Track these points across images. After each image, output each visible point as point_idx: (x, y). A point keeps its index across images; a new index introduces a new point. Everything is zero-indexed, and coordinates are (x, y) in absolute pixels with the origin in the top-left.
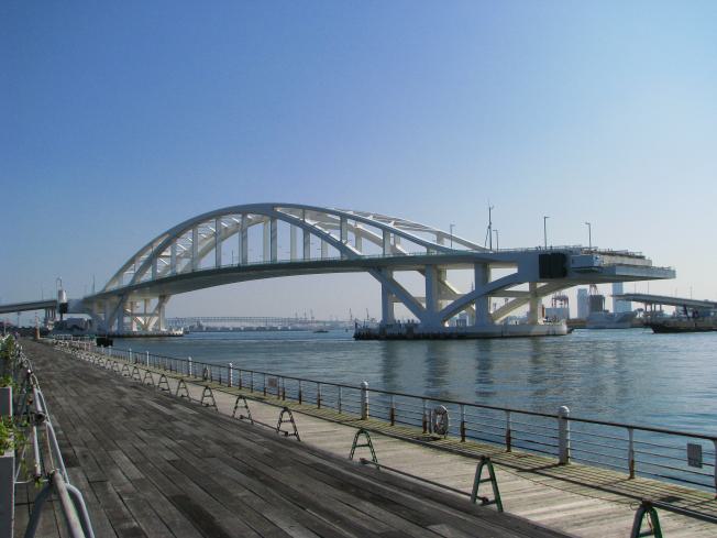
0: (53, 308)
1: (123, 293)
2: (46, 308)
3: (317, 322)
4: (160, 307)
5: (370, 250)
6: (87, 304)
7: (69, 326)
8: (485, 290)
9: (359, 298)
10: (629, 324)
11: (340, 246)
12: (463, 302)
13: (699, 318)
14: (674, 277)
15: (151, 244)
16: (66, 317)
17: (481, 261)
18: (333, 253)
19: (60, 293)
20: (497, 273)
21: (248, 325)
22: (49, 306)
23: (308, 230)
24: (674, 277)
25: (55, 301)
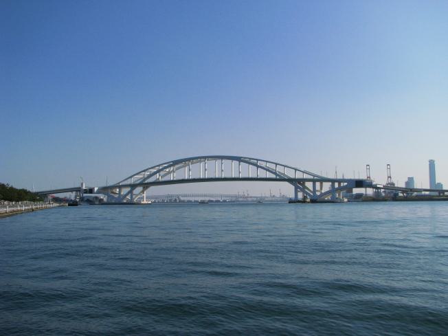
0: (79, 191)
1: (133, 186)
2: (77, 191)
3: (251, 197)
4: (143, 192)
5: (290, 174)
6: (104, 190)
7: (85, 199)
8: (333, 190)
9: (288, 190)
10: (360, 200)
11: (275, 173)
12: (327, 193)
13: (437, 195)
14: (412, 178)
15: (159, 166)
16: (85, 195)
17: (333, 181)
18: (273, 176)
19: (82, 184)
21: (203, 199)
22: (78, 190)
23: (258, 167)
24: (412, 178)
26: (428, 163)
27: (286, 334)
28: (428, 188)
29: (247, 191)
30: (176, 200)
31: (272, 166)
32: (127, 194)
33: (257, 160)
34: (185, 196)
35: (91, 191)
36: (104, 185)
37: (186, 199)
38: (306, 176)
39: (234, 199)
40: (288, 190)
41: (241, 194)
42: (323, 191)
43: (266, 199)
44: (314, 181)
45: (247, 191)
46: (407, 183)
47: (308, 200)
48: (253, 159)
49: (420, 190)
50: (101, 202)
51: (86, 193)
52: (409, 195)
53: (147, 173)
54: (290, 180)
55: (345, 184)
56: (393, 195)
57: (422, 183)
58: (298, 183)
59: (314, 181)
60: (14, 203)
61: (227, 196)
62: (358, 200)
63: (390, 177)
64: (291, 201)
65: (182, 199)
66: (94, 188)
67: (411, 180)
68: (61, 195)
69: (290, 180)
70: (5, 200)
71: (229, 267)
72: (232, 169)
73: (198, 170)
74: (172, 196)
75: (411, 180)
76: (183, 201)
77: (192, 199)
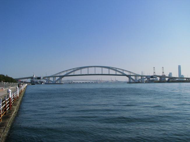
0: (32, 78)
2: (31, 78)
3: (103, 81)
5: (127, 73)
13: (181, 80)
14: (171, 73)
17: (141, 76)
19: (34, 75)
20: (144, 77)
21: (83, 82)
22: (32, 78)
24: (171, 73)
25: (33, 77)
26: (178, 67)
27: (103, 141)
28: (178, 76)
29: (101, 78)
30: (71, 82)
31: (121, 71)
32: (46, 79)
33: (123, 70)
34: (75, 80)
35: (39, 78)
36: (45, 76)
37: (76, 82)
38: (131, 74)
39: (95, 82)
40: (126, 79)
41: (99, 79)
42: (56, 80)
43: (109, 82)
44: (135, 76)
45: (101, 78)
46: (169, 75)
47: (24, 98)
48: (126, 71)
49: (175, 78)
50: (37, 83)
51: (36, 79)
52: (172, 80)
53: (69, 71)
54: (127, 76)
55: (145, 77)
56: (162, 80)
57: (175, 75)
58: (129, 76)
59: (135, 76)
60: (13, 83)
61: (93, 80)
62: (152, 82)
63: (155, 73)
64: (128, 83)
65: (74, 82)
66: (41, 77)
67: (170, 74)
68: (24, 80)
69: (127, 76)
70: (6, 82)
71: (94, 105)
72: (106, 71)
73: (85, 71)
74: (69, 80)
75: (170, 74)
76: (75, 83)
77: (79, 82)
